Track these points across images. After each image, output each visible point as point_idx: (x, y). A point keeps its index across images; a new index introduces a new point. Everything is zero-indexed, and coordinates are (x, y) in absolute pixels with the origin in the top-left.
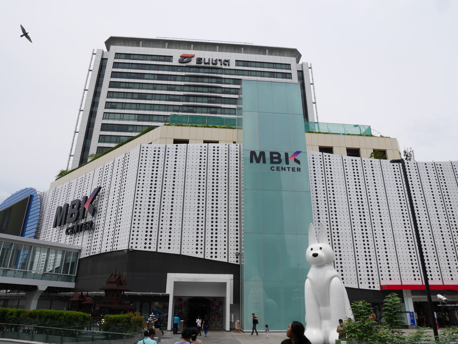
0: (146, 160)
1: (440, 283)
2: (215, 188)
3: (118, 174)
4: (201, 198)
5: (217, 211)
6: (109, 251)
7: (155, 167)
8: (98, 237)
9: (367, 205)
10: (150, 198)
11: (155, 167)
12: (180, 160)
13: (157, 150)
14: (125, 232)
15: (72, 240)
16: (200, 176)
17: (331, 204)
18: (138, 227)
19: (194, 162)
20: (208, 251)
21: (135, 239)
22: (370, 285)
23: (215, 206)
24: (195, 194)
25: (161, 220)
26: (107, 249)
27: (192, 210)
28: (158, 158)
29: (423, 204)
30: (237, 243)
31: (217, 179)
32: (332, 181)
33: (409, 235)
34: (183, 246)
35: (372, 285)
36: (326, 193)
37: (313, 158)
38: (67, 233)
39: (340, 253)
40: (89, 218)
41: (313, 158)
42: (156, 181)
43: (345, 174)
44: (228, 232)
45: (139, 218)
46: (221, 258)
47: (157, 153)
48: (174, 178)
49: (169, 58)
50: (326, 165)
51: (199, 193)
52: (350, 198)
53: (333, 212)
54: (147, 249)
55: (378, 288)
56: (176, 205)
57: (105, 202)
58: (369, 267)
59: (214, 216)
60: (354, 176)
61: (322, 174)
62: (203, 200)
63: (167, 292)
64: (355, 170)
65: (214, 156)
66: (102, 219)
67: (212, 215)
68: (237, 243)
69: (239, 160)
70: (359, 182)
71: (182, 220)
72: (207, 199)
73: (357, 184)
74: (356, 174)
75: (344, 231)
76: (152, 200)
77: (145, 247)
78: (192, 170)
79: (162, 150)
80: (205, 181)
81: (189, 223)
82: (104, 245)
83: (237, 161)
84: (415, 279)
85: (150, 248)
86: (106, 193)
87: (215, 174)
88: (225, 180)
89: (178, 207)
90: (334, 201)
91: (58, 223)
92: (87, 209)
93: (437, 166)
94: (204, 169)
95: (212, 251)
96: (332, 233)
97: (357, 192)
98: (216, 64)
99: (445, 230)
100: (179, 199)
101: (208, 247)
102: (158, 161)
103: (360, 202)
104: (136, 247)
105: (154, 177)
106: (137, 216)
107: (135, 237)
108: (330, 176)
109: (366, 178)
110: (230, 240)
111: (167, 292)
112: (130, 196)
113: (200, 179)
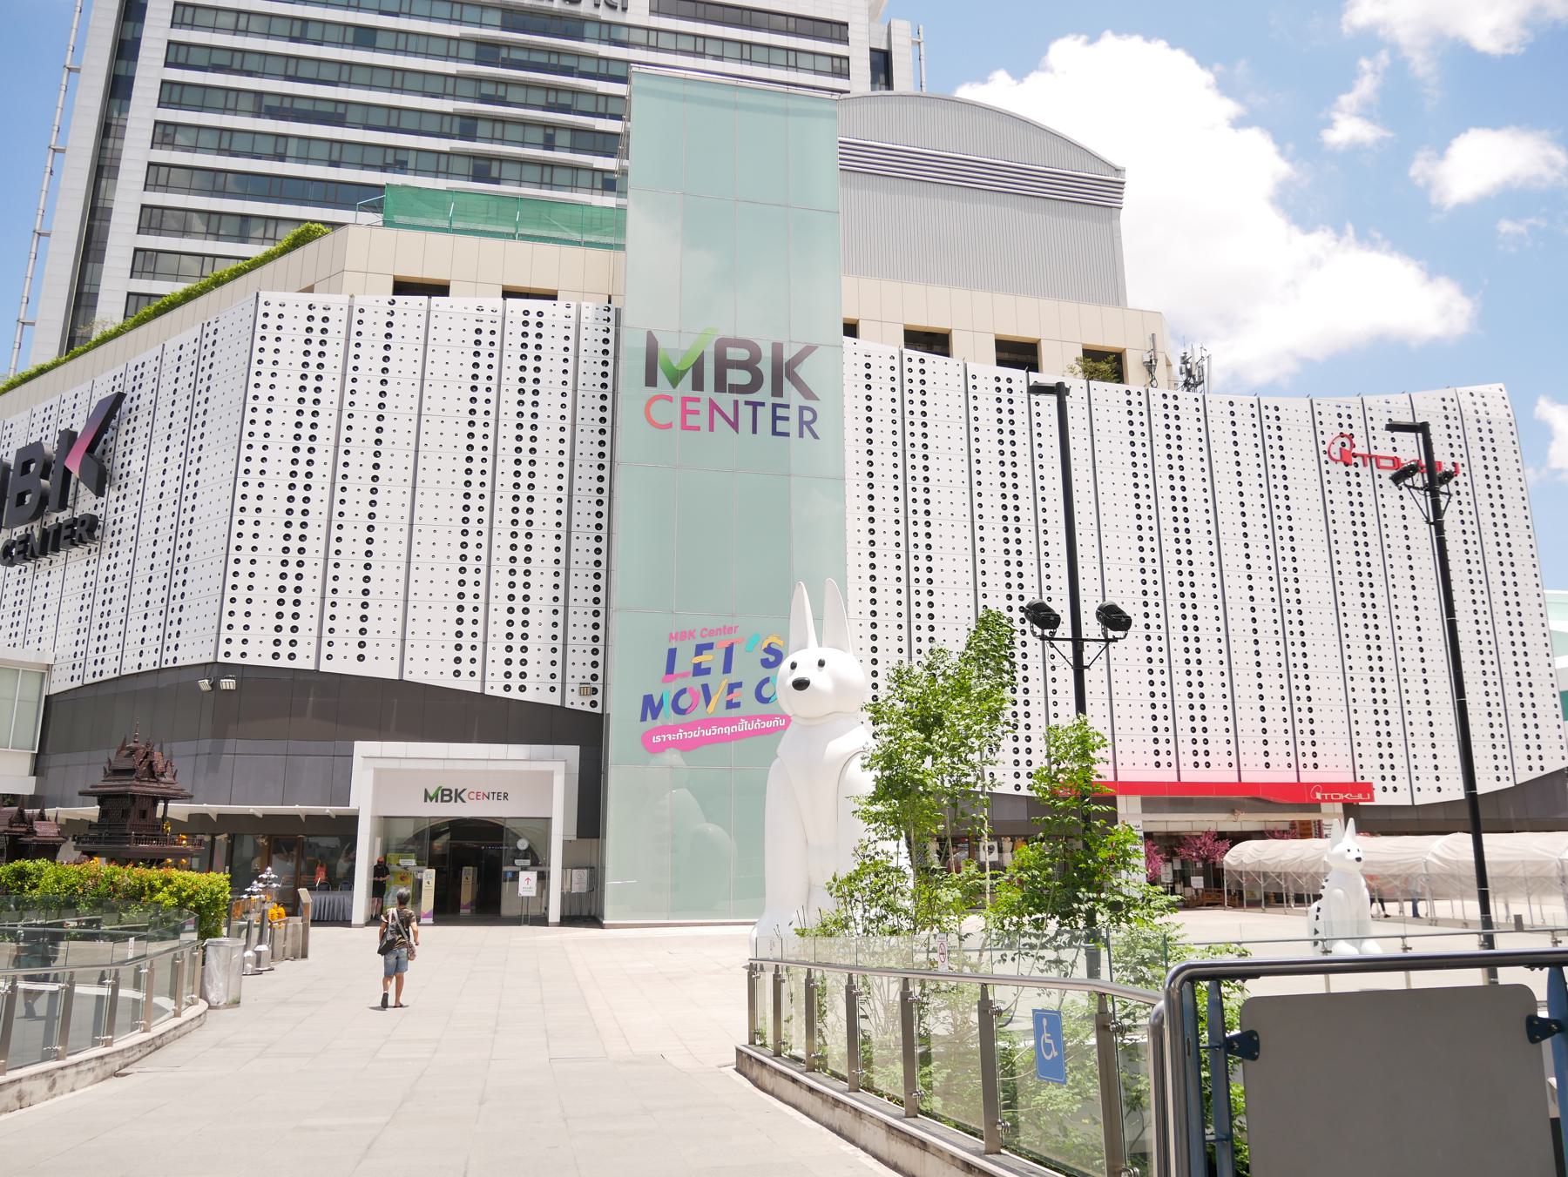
0: (248, 614)
1: (1230, 777)
2: (525, 456)
3: (176, 398)
4: (477, 454)
5: (526, 611)
6: (151, 667)
7: (316, 341)
8: (115, 584)
10: (292, 486)
11: (312, 377)
12: (401, 354)
13: (319, 314)
14: (203, 604)
15: (26, 597)
17: (915, 523)
19: (450, 364)
21: (238, 628)
31: (529, 535)
32: (925, 446)
34: (409, 652)
37: (868, 366)
39: (930, 587)
40: (85, 503)
41: (868, 366)
42: (319, 378)
44: (565, 645)
45: (253, 555)
46: (538, 692)
51: (466, 508)
53: (923, 581)
54: (283, 662)
57: (142, 430)
59: (521, 554)
62: (479, 546)
63: (353, 806)
64: (1005, 411)
66: (129, 504)
67: (508, 662)
69: (611, 362)
72: (495, 532)
73: (1011, 524)
74: (1006, 427)
75: (950, 611)
76: (299, 493)
77: (276, 656)
78: (445, 392)
80: (484, 540)
81: (441, 440)
82: (132, 649)
84: (1158, 765)
85: (292, 656)
87: (530, 375)
88: (554, 650)
90: (924, 414)
92: (75, 474)
94: (485, 436)
97: (1003, 485)
99: (1265, 615)
101: (497, 654)
102: (314, 426)
108: (918, 429)
109: (1036, 440)
110: (571, 632)
111: (353, 806)
112: (214, 515)
113: (474, 388)
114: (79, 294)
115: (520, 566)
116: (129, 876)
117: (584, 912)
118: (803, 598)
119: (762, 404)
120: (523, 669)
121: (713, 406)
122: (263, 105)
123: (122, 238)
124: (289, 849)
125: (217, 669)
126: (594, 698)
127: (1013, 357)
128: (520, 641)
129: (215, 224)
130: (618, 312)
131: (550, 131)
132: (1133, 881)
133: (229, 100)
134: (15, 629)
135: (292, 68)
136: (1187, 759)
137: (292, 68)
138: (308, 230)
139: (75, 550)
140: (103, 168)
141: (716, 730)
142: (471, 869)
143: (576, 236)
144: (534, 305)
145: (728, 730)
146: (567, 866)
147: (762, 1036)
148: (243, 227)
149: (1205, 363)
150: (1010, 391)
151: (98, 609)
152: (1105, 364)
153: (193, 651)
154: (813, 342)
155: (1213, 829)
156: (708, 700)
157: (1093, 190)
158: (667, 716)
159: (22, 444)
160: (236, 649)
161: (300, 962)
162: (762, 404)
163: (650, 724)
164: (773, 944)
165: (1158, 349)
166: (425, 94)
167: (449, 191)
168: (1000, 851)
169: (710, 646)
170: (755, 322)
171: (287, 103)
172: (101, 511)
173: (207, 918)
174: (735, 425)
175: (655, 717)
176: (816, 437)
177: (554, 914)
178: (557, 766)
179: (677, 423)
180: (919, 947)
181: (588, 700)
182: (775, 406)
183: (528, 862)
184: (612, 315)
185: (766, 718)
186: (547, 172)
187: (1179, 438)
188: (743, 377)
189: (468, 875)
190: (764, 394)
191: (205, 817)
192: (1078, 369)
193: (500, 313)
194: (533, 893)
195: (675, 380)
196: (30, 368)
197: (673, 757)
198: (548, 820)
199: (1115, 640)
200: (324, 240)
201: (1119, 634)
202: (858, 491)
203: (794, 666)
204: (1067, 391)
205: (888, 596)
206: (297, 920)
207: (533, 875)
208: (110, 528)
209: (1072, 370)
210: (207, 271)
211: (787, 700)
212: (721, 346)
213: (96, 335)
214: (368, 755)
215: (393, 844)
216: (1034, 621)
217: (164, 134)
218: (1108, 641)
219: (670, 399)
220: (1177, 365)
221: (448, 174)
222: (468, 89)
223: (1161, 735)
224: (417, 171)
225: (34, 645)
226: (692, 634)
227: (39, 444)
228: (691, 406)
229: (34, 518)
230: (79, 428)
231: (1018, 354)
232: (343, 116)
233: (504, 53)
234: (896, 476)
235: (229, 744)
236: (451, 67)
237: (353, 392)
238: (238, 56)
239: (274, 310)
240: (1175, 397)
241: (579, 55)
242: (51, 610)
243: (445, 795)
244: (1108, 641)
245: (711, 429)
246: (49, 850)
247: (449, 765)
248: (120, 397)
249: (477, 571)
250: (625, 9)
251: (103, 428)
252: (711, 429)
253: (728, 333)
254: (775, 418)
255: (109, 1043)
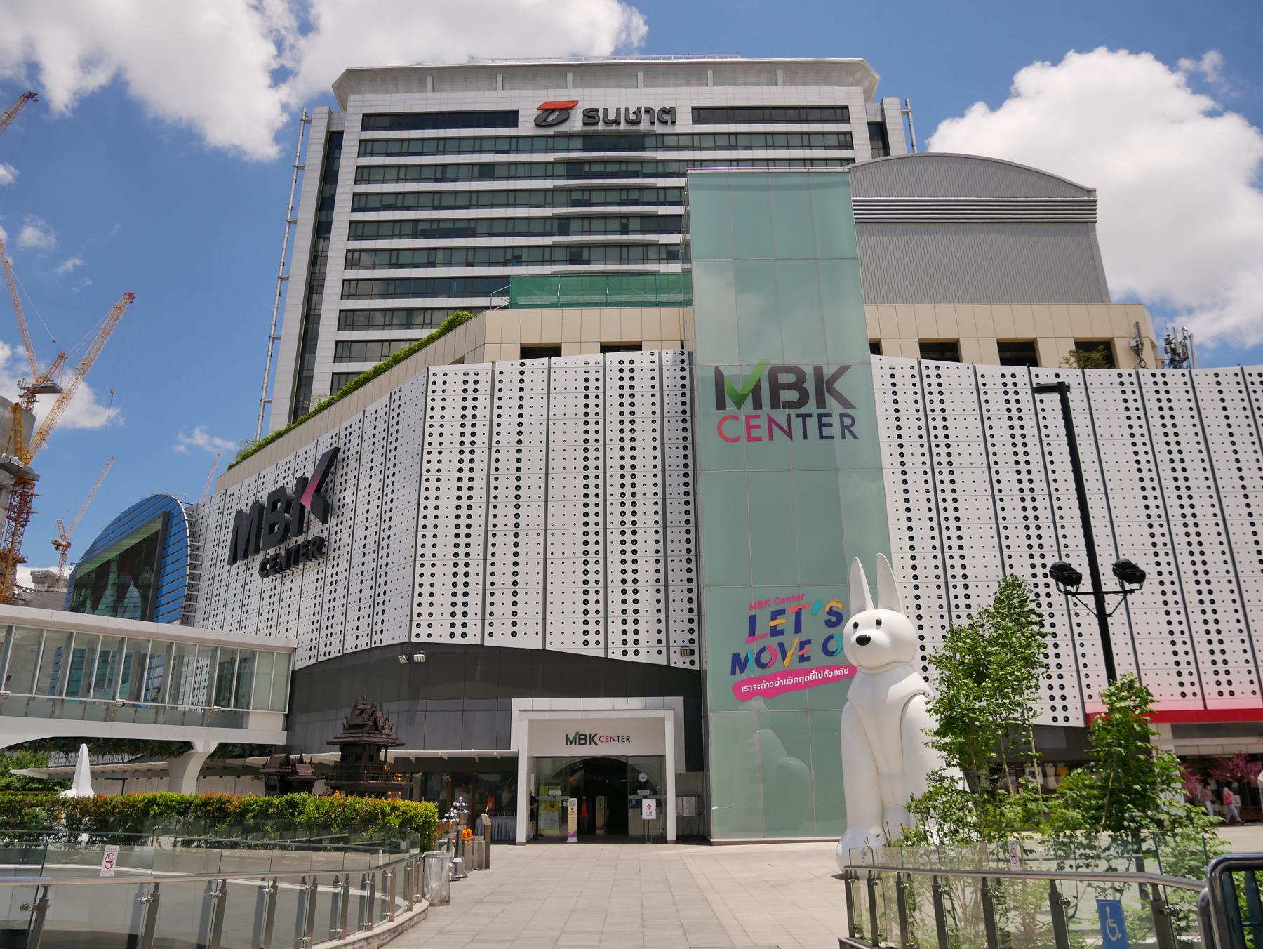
4: (592, 500)
9: (1047, 497)
13: (471, 378)
16: (586, 441)
17: (941, 473)
18: (439, 471)
19: (569, 405)
20: (616, 638)
21: (427, 575)
22: (1054, 714)
23: (629, 518)
24: (575, 607)
25: (490, 534)
26: (359, 642)
27: (569, 533)
28: (474, 425)
29: (1247, 661)
30: (691, 616)
33: (1183, 664)
35: (1060, 714)
36: (940, 556)
37: (893, 376)
38: (264, 572)
40: (315, 529)
41: (893, 376)
43: (990, 466)
44: (667, 616)
47: (470, 386)
48: (518, 497)
49: (510, 118)
50: (943, 491)
51: (586, 432)
52: (995, 454)
53: (948, 492)
54: (458, 640)
55: (1077, 722)
56: (527, 549)
58: (1058, 698)
60: (1010, 418)
61: (919, 419)
62: (597, 514)
63: (513, 749)
65: (622, 413)
66: (345, 527)
68: (691, 616)
69: (688, 393)
70: (1019, 410)
71: (545, 589)
75: (981, 571)
77: (452, 635)
79: (484, 379)
82: (351, 635)
83: (683, 395)
84: (1183, 695)
85: (464, 635)
86: (352, 460)
87: (628, 462)
88: (655, 448)
89: (533, 554)
91: (241, 552)
92: (308, 508)
93: (1249, 380)
95: (624, 627)
96: (949, 578)
97: (1020, 481)
98: (637, 123)
100: (534, 505)
101: (615, 626)
103: (1027, 491)
104: (429, 635)
105: (467, 451)
106: (430, 527)
107: (425, 610)
111: (513, 749)
112: (402, 561)
114: (300, 378)
115: (463, 531)
116: (367, 804)
117: (695, 832)
118: (859, 570)
119: (810, 415)
120: (636, 637)
121: (771, 421)
122: (418, 229)
123: (328, 334)
124: (467, 784)
125: (411, 647)
126: (692, 658)
127: (1014, 355)
128: (630, 616)
129: (389, 318)
130: (690, 354)
131: (624, 221)
132: (1172, 800)
133: (396, 230)
134: (329, 623)
135: (437, 201)
136: (1211, 689)
137: (437, 201)
138: (458, 316)
139: (309, 563)
140: (314, 287)
141: (792, 680)
142: (604, 799)
143: (651, 297)
144: (626, 356)
145: (802, 680)
146: (680, 794)
147: (860, 930)
148: (409, 318)
149: (1188, 342)
150: (1028, 463)
151: (326, 606)
152: (1095, 353)
153: (393, 635)
154: (846, 362)
155: (1244, 751)
156: (784, 656)
157: (1069, 210)
158: (752, 670)
159: (271, 489)
160: (424, 631)
161: (484, 872)
162: (810, 415)
163: (740, 677)
164: (864, 854)
165: (1143, 333)
166: (532, 206)
167: (555, 275)
168: (1045, 775)
169: (782, 612)
170: (792, 349)
171: (435, 226)
172: (326, 533)
173: (424, 835)
174: (789, 434)
175: (742, 671)
176: (855, 437)
177: (671, 834)
178: (667, 714)
179: (744, 437)
180: (992, 857)
181: (687, 660)
182: (820, 416)
183: (647, 792)
184: (686, 357)
185: (832, 668)
186: (624, 251)
187: (1194, 516)
188: (792, 396)
189: (601, 802)
190: (811, 407)
191: (406, 759)
192: (1073, 359)
193: (602, 364)
194: (654, 817)
195: (739, 404)
196: (271, 433)
197: (758, 703)
198: (661, 758)
199: (1132, 591)
200: (470, 322)
201: (1135, 586)
202: (893, 478)
203: (856, 626)
204: (1068, 388)
205: (926, 562)
206: (481, 839)
207: (653, 802)
208: (333, 546)
209: (1067, 361)
210: (385, 352)
211: (855, 656)
212: (773, 373)
213: (312, 409)
214: (524, 709)
215: (543, 781)
216: (1058, 579)
217: (352, 260)
218: (1125, 592)
219: (736, 418)
220: (1161, 343)
221: (551, 262)
222: (562, 197)
223: (1186, 666)
224: (529, 263)
225: (283, 634)
226: (767, 603)
227: (283, 488)
228: (753, 422)
229: (281, 542)
230: (309, 475)
231: (1019, 353)
232: (474, 229)
233: (586, 168)
234: (924, 463)
235: (422, 703)
236: (549, 184)
237: (498, 433)
238: (400, 197)
239: (439, 379)
240: (1164, 375)
241: (642, 161)
242: (294, 608)
243: (582, 739)
244: (1125, 592)
245: (771, 438)
246: (306, 786)
247: (584, 715)
248: (337, 450)
249: (597, 543)
250: (674, 123)
251: (325, 475)
252: (771, 438)
253: (777, 362)
254: (821, 425)
255: (370, 928)
